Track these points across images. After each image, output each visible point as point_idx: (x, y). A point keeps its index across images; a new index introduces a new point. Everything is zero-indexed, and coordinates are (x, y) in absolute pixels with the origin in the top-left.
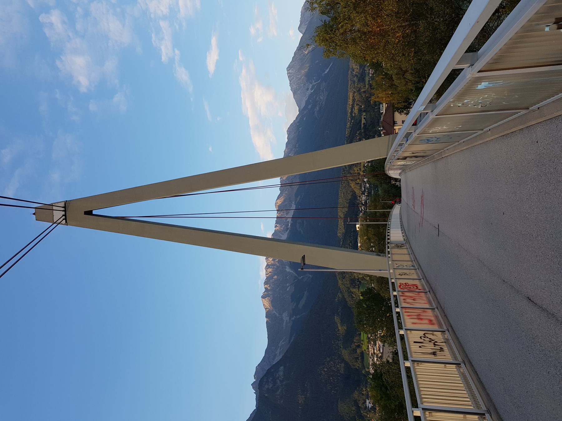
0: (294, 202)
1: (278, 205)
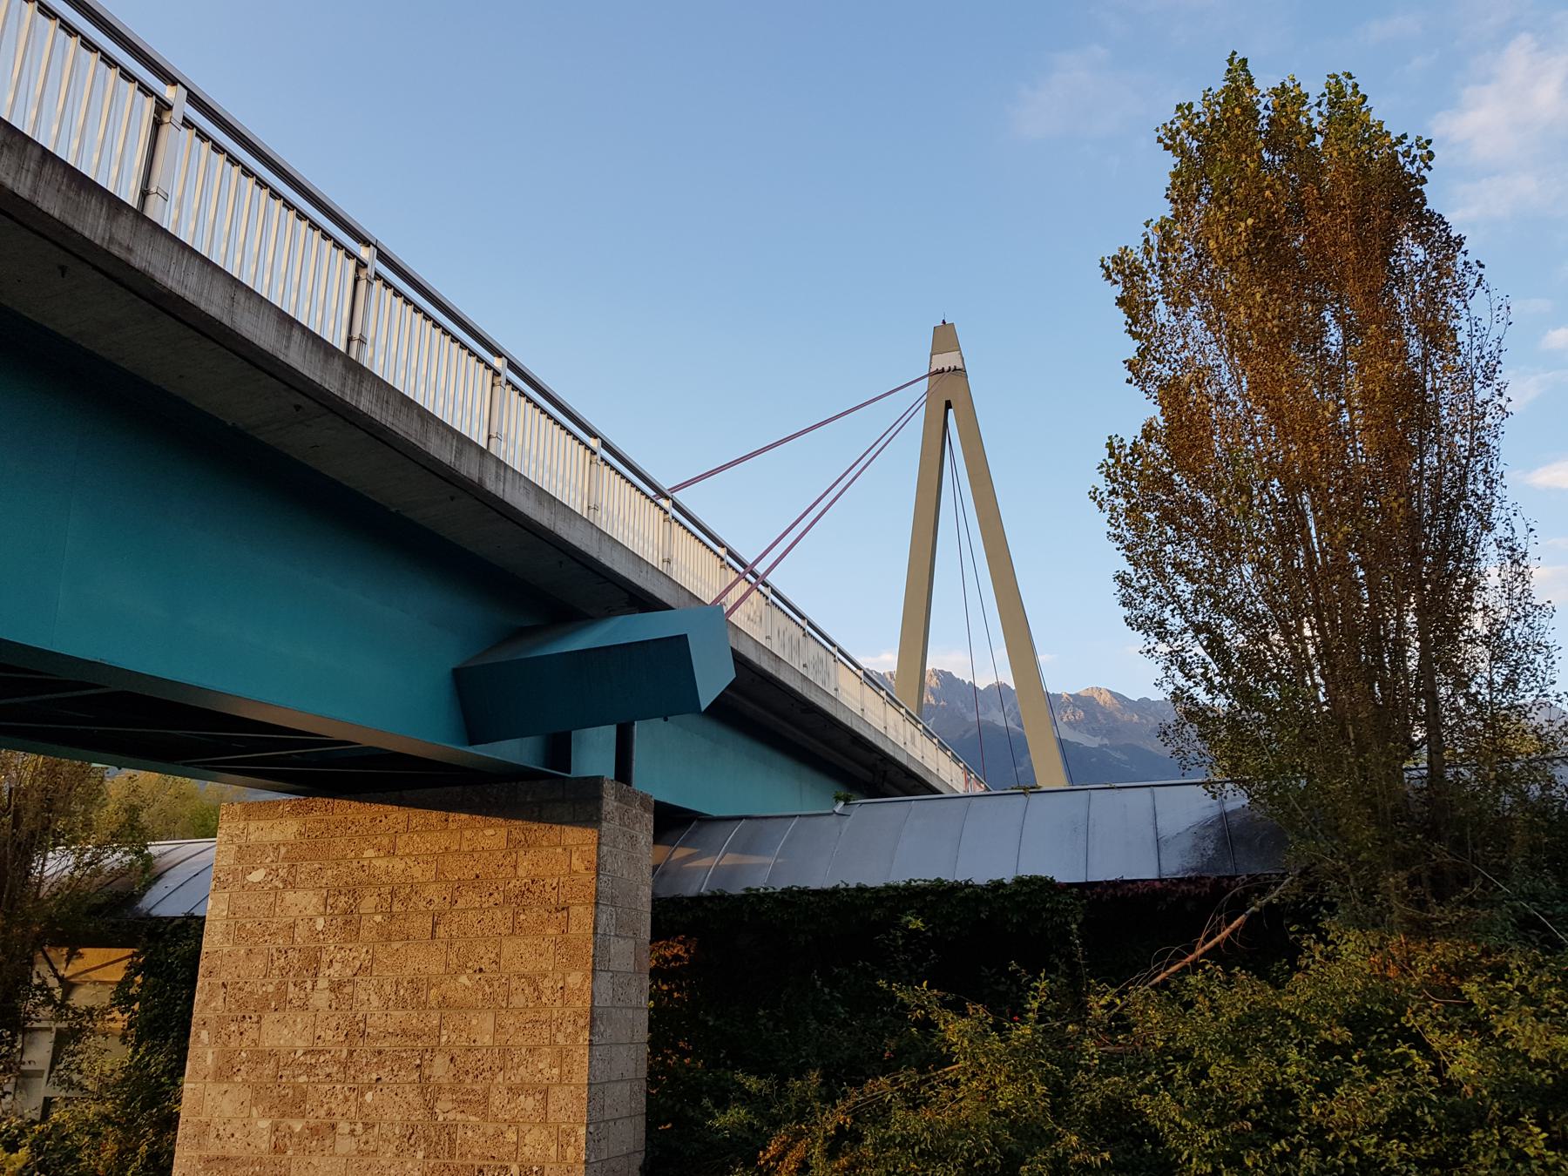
0: (1106, 741)
1: (1095, 696)
